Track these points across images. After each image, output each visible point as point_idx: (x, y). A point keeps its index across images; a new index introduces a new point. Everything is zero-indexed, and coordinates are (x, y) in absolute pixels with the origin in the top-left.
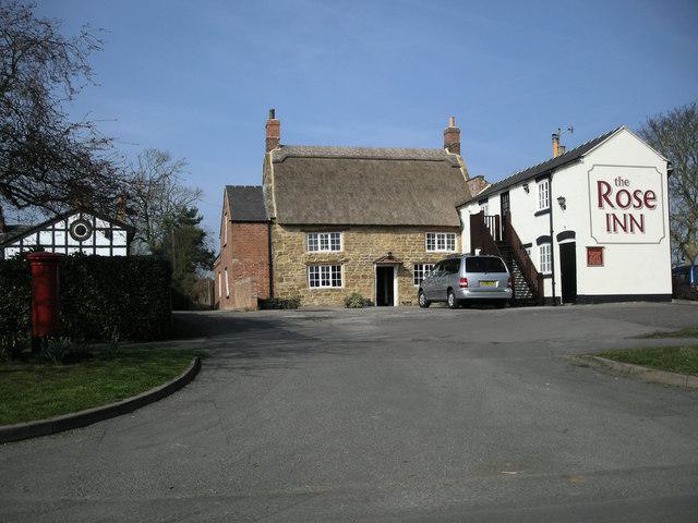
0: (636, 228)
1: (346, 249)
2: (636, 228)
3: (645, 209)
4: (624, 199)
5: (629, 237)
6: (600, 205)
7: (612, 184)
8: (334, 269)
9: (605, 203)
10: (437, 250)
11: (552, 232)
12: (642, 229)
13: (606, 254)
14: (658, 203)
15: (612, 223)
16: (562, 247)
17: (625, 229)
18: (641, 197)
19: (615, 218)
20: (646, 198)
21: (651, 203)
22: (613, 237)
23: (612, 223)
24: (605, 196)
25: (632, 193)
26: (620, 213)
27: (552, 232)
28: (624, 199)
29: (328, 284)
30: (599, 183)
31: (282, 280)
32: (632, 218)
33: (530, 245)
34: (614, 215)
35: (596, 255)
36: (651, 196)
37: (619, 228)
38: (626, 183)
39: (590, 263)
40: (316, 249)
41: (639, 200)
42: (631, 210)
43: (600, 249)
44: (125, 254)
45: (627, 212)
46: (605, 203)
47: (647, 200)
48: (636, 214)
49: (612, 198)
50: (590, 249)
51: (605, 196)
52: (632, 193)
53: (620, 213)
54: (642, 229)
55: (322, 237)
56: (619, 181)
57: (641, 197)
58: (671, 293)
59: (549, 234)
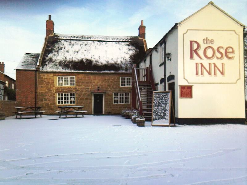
0: (218, 73)
1: (77, 85)
2: (218, 73)
3: (225, 60)
4: (210, 53)
5: (212, 79)
6: (191, 57)
7: (201, 43)
8: (126, 95)
9: (195, 55)
10: (126, 86)
11: (165, 75)
12: (222, 73)
13: (195, 91)
14: (236, 55)
15: (200, 69)
16: (169, 84)
17: (209, 73)
18: (223, 51)
19: (202, 65)
20: (226, 52)
21: (230, 55)
22: (200, 79)
23: (200, 69)
24: (195, 51)
25: (216, 49)
26: (206, 62)
27: (165, 75)
28: (210, 53)
29: (123, 102)
30: (191, 42)
31: (42, 101)
32: (215, 66)
33: (158, 84)
34: (201, 64)
35: (187, 91)
36: (230, 50)
37: (205, 72)
38: (212, 41)
39: (182, 96)
40: (124, 85)
41: (221, 53)
42: (215, 60)
43: (190, 88)
44: (1, 88)
45: (212, 61)
46: (195, 55)
47: (227, 53)
48: (219, 63)
49: (201, 52)
50: (182, 87)
51: (195, 51)
52: (216, 49)
53: (206, 62)
54: (222, 73)
55: (122, 79)
56: (206, 40)
57: (223, 51)
58: (179, 117)
59: (164, 77)
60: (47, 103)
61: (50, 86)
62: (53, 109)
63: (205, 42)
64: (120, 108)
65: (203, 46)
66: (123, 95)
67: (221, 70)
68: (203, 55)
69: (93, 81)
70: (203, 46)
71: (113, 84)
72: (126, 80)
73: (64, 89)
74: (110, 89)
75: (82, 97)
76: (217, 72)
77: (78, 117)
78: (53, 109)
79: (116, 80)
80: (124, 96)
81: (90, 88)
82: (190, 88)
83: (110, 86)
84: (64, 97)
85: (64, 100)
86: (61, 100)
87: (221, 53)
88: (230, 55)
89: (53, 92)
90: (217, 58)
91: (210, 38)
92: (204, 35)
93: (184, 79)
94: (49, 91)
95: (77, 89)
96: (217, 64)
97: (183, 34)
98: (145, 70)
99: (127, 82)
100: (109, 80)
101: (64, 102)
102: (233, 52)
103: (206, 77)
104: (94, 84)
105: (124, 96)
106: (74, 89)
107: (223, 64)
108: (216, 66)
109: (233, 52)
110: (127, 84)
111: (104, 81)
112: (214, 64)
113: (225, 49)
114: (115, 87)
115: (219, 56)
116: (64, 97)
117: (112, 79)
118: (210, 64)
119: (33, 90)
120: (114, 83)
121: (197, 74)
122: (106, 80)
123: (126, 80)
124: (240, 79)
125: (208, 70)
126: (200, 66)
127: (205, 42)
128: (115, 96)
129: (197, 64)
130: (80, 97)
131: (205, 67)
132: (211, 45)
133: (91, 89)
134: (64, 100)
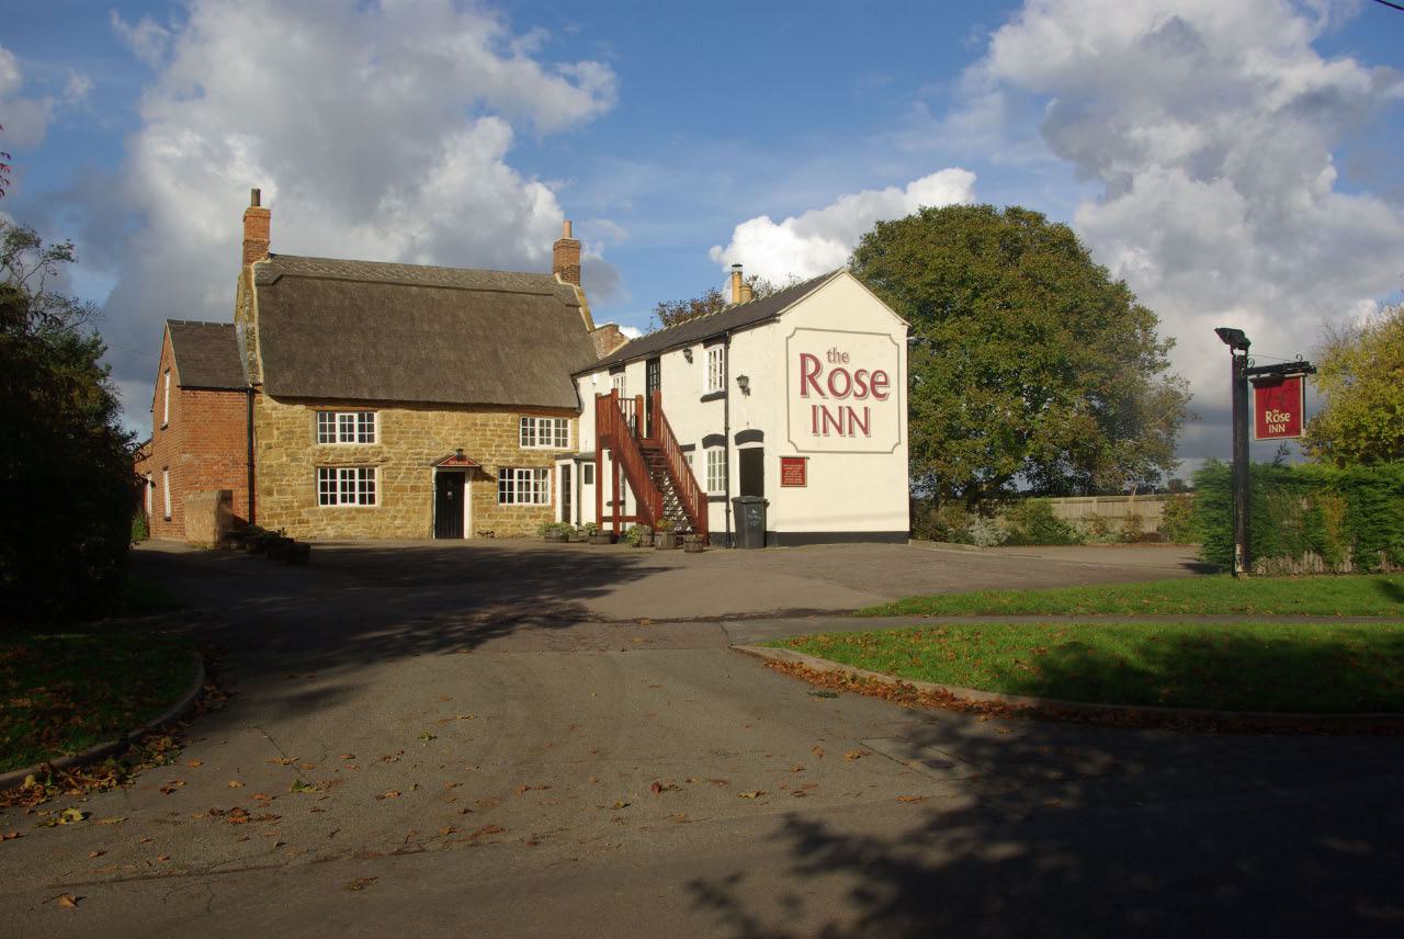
1: (384, 441)
3: (871, 401)
5: (845, 442)
6: (804, 392)
7: (823, 359)
8: (362, 475)
9: (810, 388)
11: (727, 429)
12: (866, 430)
14: (892, 390)
15: (821, 421)
17: (840, 429)
18: (866, 380)
19: (826, 412)
20: (873, 383)
21: (881, 390)
22: (823, 442)
23: (821, 421)
24: (811, 377)
25: (852, 375)
26: (833, 405)
27: (727, 429)
30: (804, 357)
32: (851, 413)
34: (823, 407)
35: (794, 470)
36: (882, 379)
37: (832, 429)
38: (844, 357)
41: (862, 385)
42: (850, 401)
43: (801, 461)
45: (844, 403)
46: (810, 388)
47: (875, 385)
49: (822, 381)
51: (811, 377)
52: (852, 375)
53: (833, 405)
54: (866, 430)
56: (834, 355)
57: (866, 380)
60: (285, 503)
61: (297, 444)
62: (308, 522)
63: (832, 357)
64: (519, 517)
65: (827, 368)
66: (352, 475)
67: (863, 423)
68: (826, 384)
69: (434, 430)
70: (827, 368)
71: (497, 439)
72: (338, 423)
73: (341, 456)
74: (490, 455)
75: (399, 480)
76: (856, 426)
77: (728, 516)
78: (308, 522)
79: (508, 425)
80: (357, 480)
81: (426, 451)
82: (801, 461)
83: (487, 446)
84: (339, 480)
85: (339, 493)
86: (326, 483)
87: (862, 385)
88: (881, 390)
89: (304, 464)
90: (856, 395)
91: (841, 350)
92: (833, 341)
93: (789, 441)
94: (292, 461)
95: (386, 455)
96: (828, 409)
97: (787, 339)
98: (633, 402)
99: (343, 428)
100: (486, 425)
101: (339, 498)
102: (885, 383)
103: (834, 439)
104: (437, 439)
105: (357, 480)
106: (374, 454)
107: (866, 409)
108: (855, 416)
109: (885, 383)
110: (343, 438)
111: (470, 429)
112: (849, 408)
113: (871, 374)
114: (504, 448)
115: (859, 390)
116: (339, 480)
117: (497, 422)
118: (840, 408)
119: (243, 455)
120: (500, 436)
121: (815, 431)
122: (475, 425)
123: (338, 423)
124: (899, 443)
125: (838, 423)
126: (820, 412)
127: (832, 357)
128: (370, 483)
129: (814, 407)
130: (392, 483)
131: (833, 415)
132: (842, 366)
133: (427, 455)
134: (339, 493)
